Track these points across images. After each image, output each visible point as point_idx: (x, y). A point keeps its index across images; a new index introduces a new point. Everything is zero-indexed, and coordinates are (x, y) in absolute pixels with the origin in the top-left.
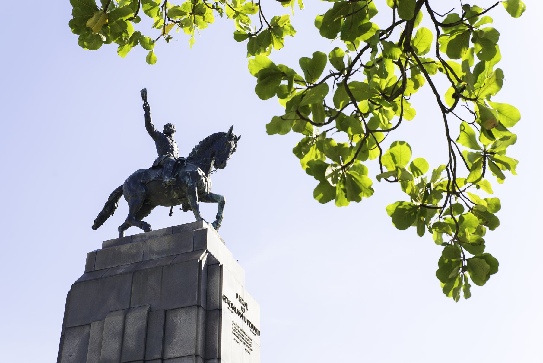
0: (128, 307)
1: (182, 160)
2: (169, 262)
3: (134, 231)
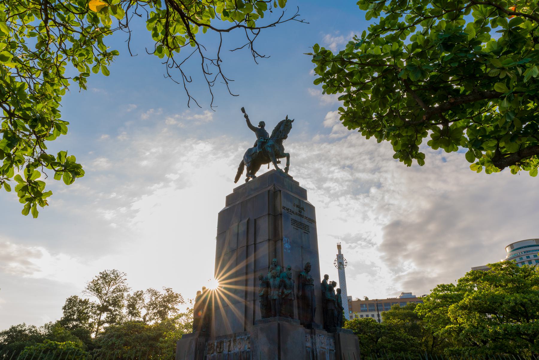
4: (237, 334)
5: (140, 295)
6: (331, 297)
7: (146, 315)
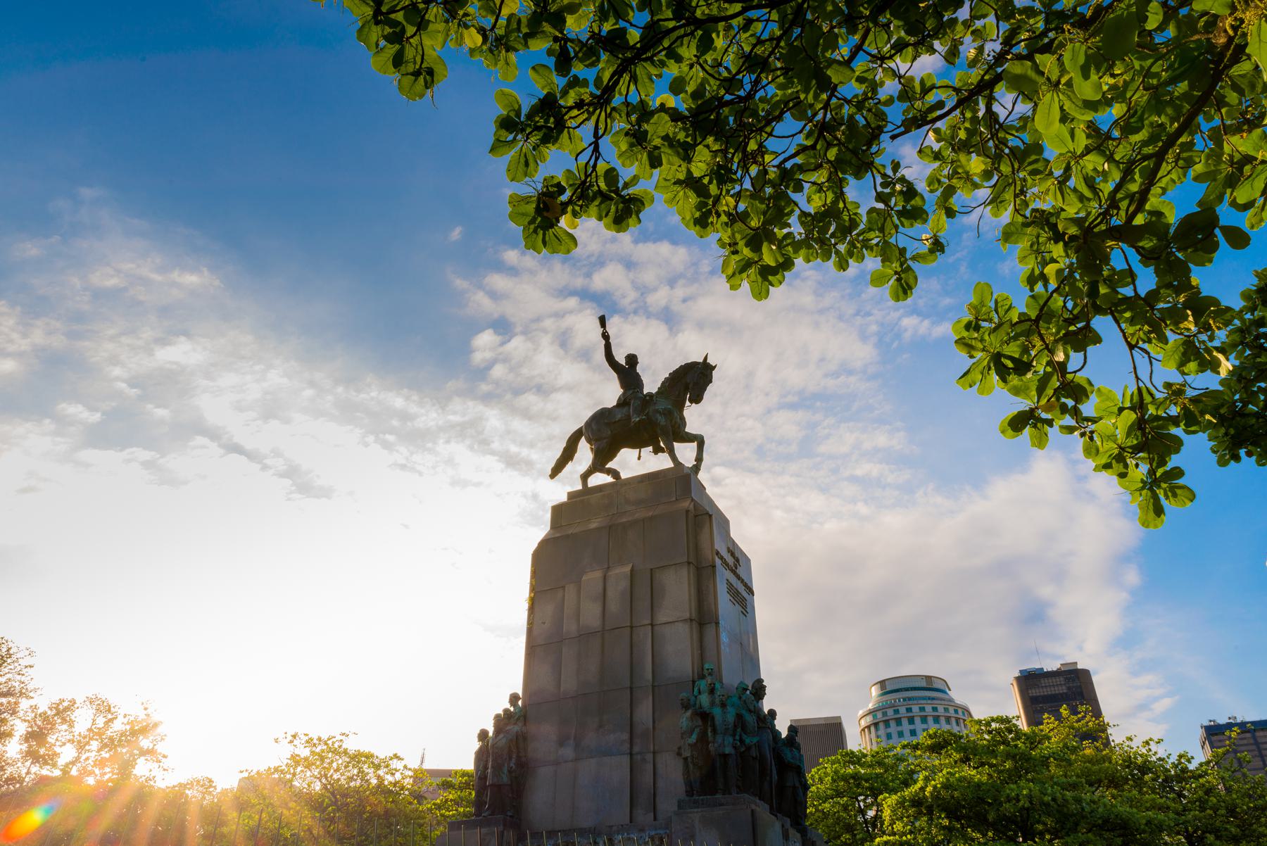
0: (606, 566)
1: (650, 395)
2: (651, 514)
3: (599, 479)
4: (615, 828)
5: (67, 709)
6: (793, 758)
7: (73, 763)
